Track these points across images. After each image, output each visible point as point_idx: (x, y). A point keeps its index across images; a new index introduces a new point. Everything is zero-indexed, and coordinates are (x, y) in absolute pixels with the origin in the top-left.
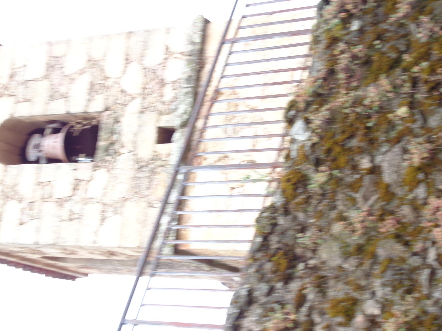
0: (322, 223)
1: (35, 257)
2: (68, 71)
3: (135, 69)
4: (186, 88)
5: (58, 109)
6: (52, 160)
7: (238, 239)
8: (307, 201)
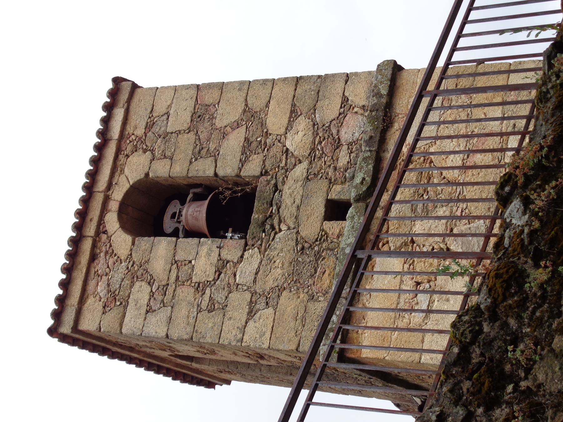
0: (540, 333)
1: (165, 354)
2: (219, 123)
3: (302, 124)
4: (366, 152)
5: (204, 169)
6: (191, 233)
7: (431, 348)
8: (522, 305)
